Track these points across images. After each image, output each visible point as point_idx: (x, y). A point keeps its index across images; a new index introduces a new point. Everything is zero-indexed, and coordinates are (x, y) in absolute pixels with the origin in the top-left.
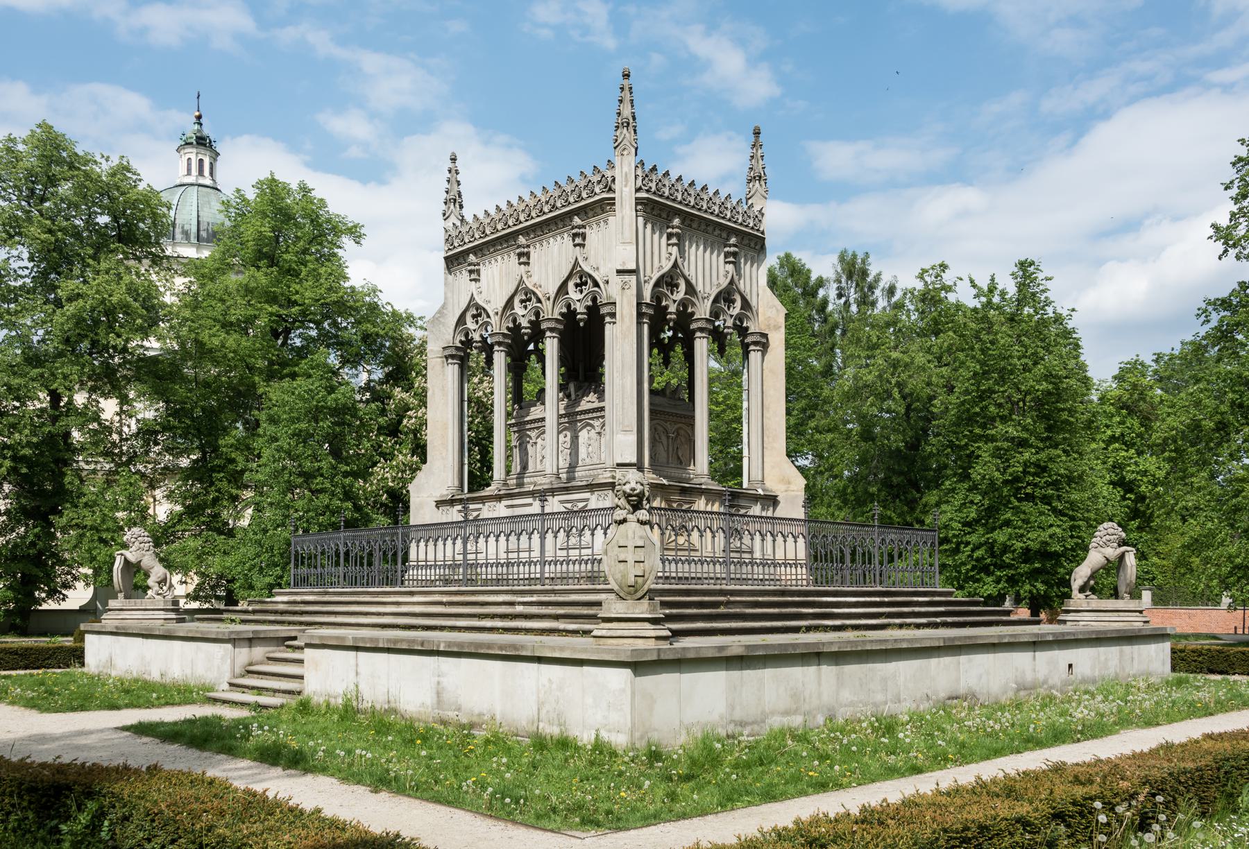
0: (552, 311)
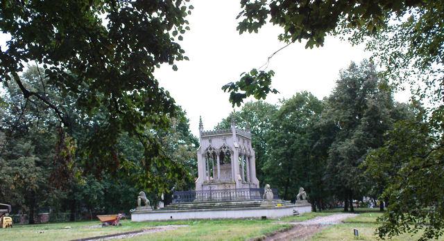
0: (217, 152)
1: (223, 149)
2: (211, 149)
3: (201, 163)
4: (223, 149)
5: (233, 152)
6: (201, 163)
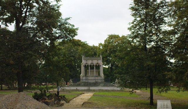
0: (95, 65)
1: (97, 64)
2: (92, 64)
3: (83, 68)
4: (97, 64)
5: (83, 66)
6: (83, 68)
